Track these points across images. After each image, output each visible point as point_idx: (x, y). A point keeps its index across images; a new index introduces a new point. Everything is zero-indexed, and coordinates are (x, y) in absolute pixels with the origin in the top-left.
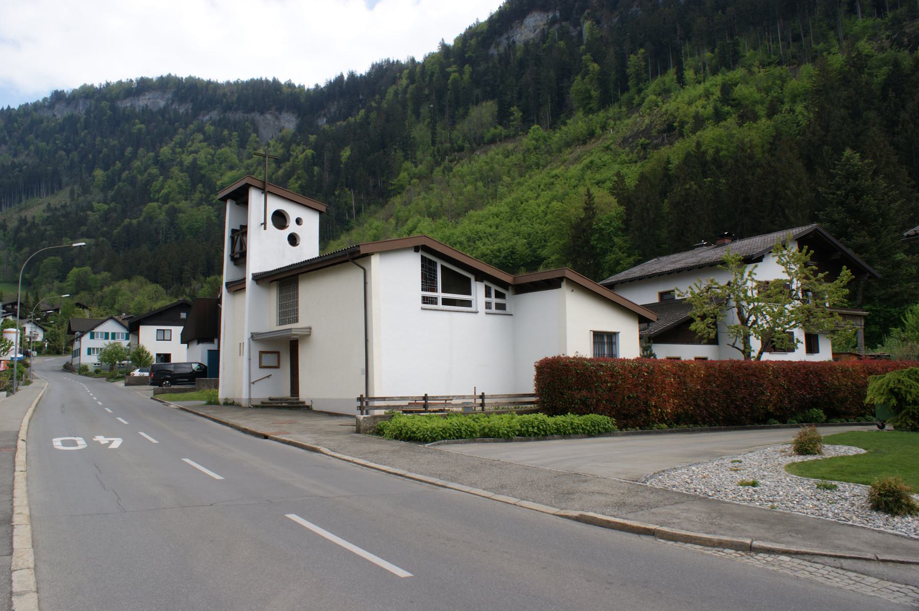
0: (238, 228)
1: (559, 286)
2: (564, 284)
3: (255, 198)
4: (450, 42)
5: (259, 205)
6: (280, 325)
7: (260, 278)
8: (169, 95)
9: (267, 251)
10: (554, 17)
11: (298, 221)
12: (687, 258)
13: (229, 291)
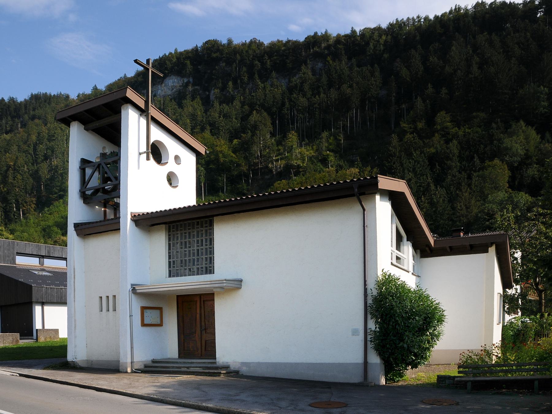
4: (358, 30)
7: (147, 222)
12: (80, 379)
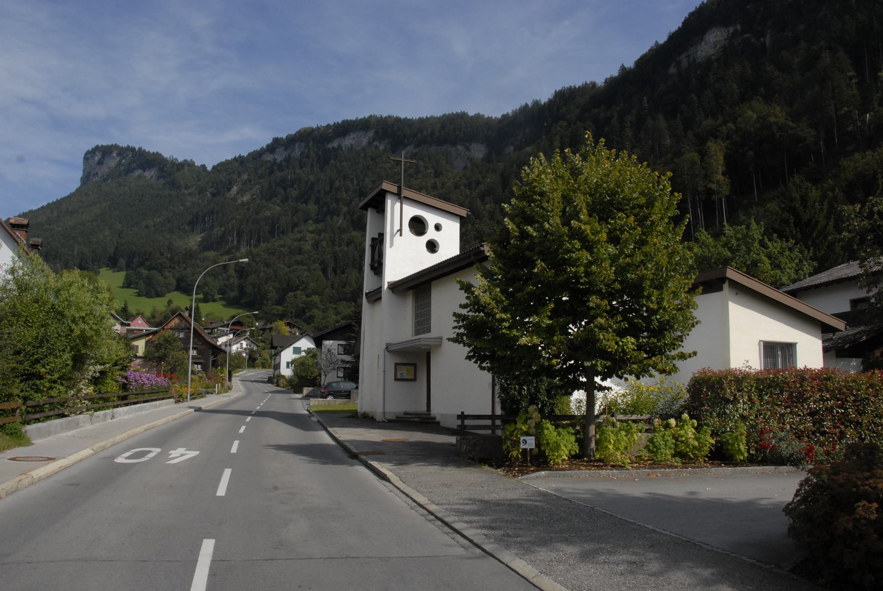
0: (377, 237)
1: (720, 289)
2: (726, 286)
3: (392, 207)
5: (400, 213)
6: (416, 335)
7: (395, 287)
8: (371, 134)
9: (404, 257)
10: (736, 31)
11: (438, 227)
13: (369, 302)
